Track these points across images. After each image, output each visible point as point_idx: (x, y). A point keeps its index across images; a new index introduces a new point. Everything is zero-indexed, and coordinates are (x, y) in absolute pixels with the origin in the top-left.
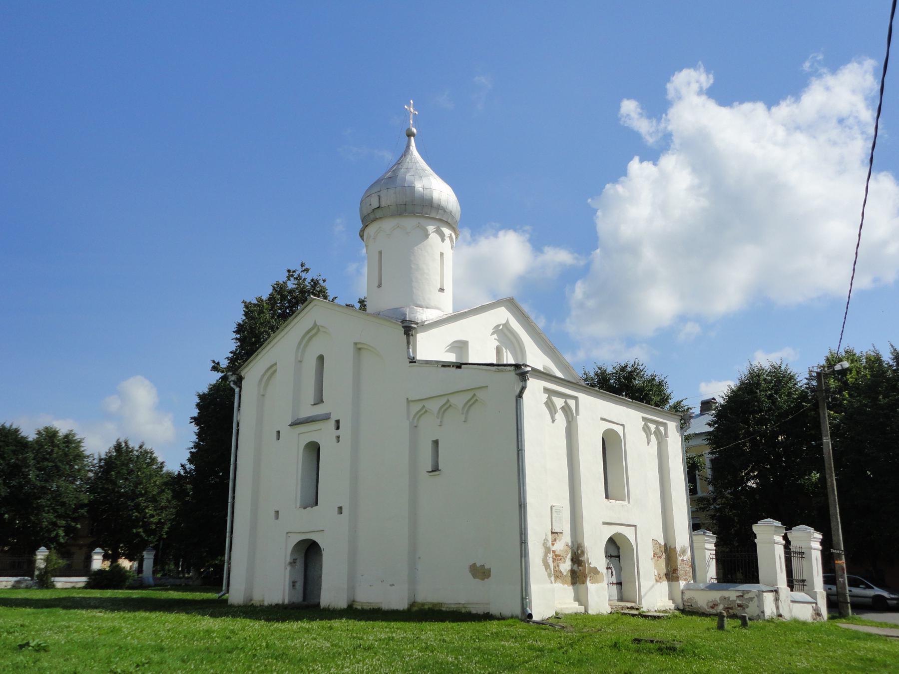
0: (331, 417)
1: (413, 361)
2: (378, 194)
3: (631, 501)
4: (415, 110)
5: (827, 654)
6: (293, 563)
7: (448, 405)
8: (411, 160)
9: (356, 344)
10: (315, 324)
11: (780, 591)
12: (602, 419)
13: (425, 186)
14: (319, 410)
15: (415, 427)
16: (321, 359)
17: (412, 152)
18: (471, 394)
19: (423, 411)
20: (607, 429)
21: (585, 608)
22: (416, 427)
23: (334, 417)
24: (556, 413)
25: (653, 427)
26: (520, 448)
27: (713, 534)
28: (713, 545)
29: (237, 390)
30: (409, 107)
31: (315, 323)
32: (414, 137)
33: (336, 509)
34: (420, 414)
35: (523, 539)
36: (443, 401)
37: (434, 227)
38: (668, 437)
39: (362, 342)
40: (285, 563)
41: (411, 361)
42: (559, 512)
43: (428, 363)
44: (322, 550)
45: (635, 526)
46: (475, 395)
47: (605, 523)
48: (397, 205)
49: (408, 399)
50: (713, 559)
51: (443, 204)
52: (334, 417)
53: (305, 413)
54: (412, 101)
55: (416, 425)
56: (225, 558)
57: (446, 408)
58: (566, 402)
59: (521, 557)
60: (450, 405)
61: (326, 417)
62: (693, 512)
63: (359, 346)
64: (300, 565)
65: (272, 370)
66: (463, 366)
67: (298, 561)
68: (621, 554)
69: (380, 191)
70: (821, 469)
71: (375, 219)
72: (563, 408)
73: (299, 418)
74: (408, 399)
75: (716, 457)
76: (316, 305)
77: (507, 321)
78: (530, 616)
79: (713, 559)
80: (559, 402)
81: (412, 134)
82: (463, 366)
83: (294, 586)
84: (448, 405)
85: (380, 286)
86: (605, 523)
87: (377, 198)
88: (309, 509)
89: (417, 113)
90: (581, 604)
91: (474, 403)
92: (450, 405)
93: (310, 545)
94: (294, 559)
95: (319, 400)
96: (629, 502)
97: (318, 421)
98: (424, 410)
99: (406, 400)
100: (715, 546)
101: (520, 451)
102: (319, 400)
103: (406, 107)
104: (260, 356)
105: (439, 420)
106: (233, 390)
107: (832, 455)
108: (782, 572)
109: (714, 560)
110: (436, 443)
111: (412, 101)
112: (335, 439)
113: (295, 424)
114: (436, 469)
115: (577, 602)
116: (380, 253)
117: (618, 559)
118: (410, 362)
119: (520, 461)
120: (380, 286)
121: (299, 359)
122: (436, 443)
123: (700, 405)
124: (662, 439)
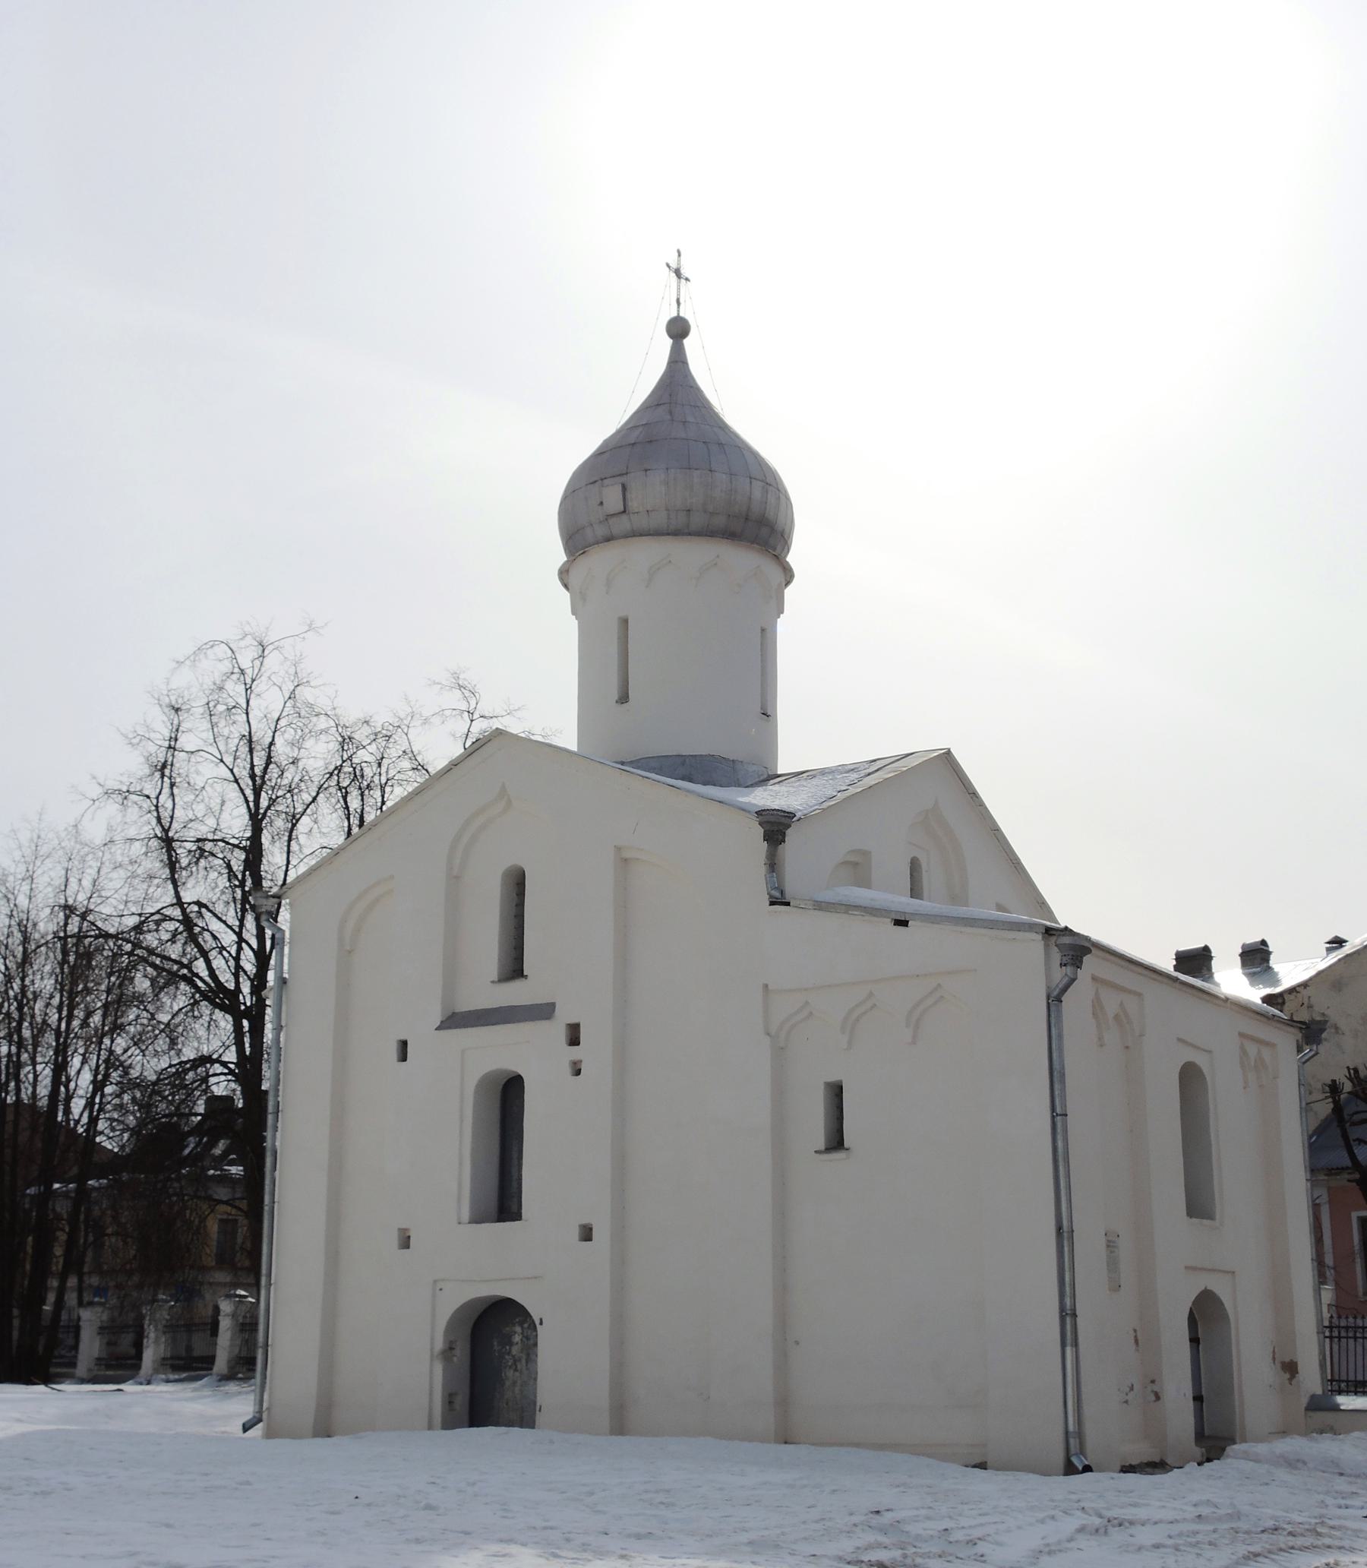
2: (623, 479)
6: (450, 1348)
9: (618, 849)
10: (503, 788)
14: (515, 994)
15: (780, 1052)
16: (517, 884)
20: (1188, 1062)
23: (564, 1016)
25: (1252, 1049)
26: (1058, 1110)
33: (576, 1233)
35: (1068, 1307)
40: (432, 1349)
44: (537, 1322)
48: (1340, 991)
52: (564, 1016)
59: (1063, 1345)
61: (544, 1012)
63: (627, 854)
64: (462, 1353)
69: (627, 473)
72: (1116, 1017)
73: (457, 1011)
75: (250, 875)
83: (450, 1403)
87: (619, 488)
95: (514, 969)
102: (514, 969)
110: (836, 1092)
112: (567, 1070)
113: (454, 1021)
114: (836, 1142)
116: (624, 698)
118: (772, 903)
119: (1059, 1137)
122: (836, 1092)
123: (1174, 963)
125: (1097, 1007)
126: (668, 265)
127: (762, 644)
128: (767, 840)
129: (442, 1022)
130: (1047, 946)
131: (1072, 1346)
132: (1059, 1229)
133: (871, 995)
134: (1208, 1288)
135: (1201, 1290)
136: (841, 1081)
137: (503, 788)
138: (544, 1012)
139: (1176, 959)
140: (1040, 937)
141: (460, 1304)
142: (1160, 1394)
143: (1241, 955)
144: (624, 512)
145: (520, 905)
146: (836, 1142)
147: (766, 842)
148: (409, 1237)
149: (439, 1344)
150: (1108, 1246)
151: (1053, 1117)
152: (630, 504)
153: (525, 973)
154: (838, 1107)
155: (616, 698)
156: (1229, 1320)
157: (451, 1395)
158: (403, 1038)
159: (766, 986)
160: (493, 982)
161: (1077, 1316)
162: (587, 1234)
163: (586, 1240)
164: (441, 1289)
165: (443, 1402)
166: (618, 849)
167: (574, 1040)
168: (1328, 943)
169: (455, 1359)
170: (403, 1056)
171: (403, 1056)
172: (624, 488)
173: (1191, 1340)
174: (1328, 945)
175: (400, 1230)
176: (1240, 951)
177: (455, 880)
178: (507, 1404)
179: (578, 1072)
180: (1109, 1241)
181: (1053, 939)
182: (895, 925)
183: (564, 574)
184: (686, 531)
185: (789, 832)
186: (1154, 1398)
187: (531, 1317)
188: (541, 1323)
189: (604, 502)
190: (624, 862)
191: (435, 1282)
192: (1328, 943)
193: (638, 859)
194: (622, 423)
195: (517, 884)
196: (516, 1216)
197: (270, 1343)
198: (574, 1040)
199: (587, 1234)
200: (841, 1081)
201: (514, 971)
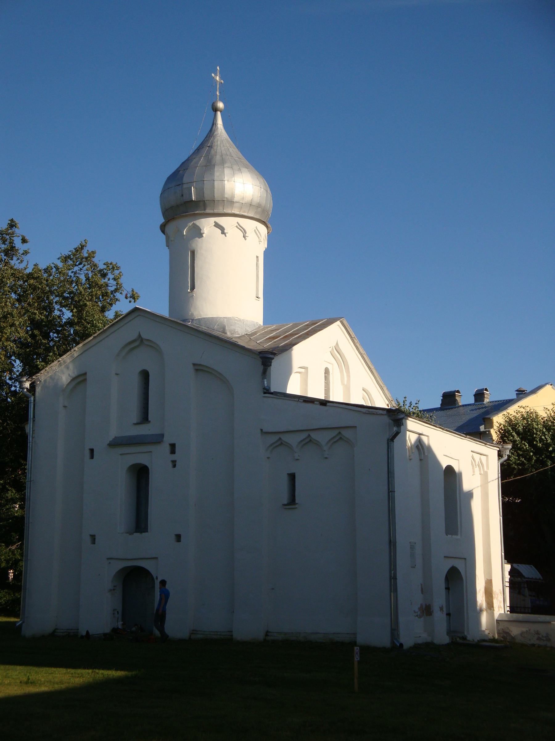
1: (267, 391)
9: (194, 365)
19: (281, 443)
20: (448, 465)
23: (168, 440)
25: (477, 457)
31: (140, 335)
36: (304, 435)
39: (202, 363)
41: (265, 391)
44: (155, 577)
45: (465, 559)
46: (340, 433)
49: (262, 430)
54: (218, 68)
56: (21, 584)
57: (309, 441)
58: (480, 459)
59: (391, 591)
60: (310, 440)
61: (157, 439)
62: (171, 451)
66: (328, 404)
70: (535, 471)
74: (262, 430)
76: (140, 315)
77: (337, 344)
82: (328, 404)
88: (128, 534)
92: (310, 440)
94: (114, 586)
95: (145, 418)
97: (145, 443)
98: (279, 443)
99: (259, 431)
102: (145, 418)
106: (28, 402)
107: (285, 335)
108: (489, 584)
109: (508, 588)
111: (218, 68)
112: (171, 465)
118: (265, 393)
123: (442, 398)
127: (257, 264)
128: (263, 365)
131: (185, 322)
132: (390, 541)
134: (454, 566)
136: (295, 473)
138: (157, 439)
143: (475, 395)
147: (263, 366)
150: (411, 548)
151: (389, 493)
153: (149, 420)
156: (463, 580)
161: (397, 579)
167: (173, 451)
168: (516, 391)
173: (446, 588)
174: (517, 392)
176: (475, 393)
179: (174, 466)
180: (411, 546)
182: (320, 405)
183: (163, 228)
185: (273, 361)
196: (145, 530)
198: (173, 451)
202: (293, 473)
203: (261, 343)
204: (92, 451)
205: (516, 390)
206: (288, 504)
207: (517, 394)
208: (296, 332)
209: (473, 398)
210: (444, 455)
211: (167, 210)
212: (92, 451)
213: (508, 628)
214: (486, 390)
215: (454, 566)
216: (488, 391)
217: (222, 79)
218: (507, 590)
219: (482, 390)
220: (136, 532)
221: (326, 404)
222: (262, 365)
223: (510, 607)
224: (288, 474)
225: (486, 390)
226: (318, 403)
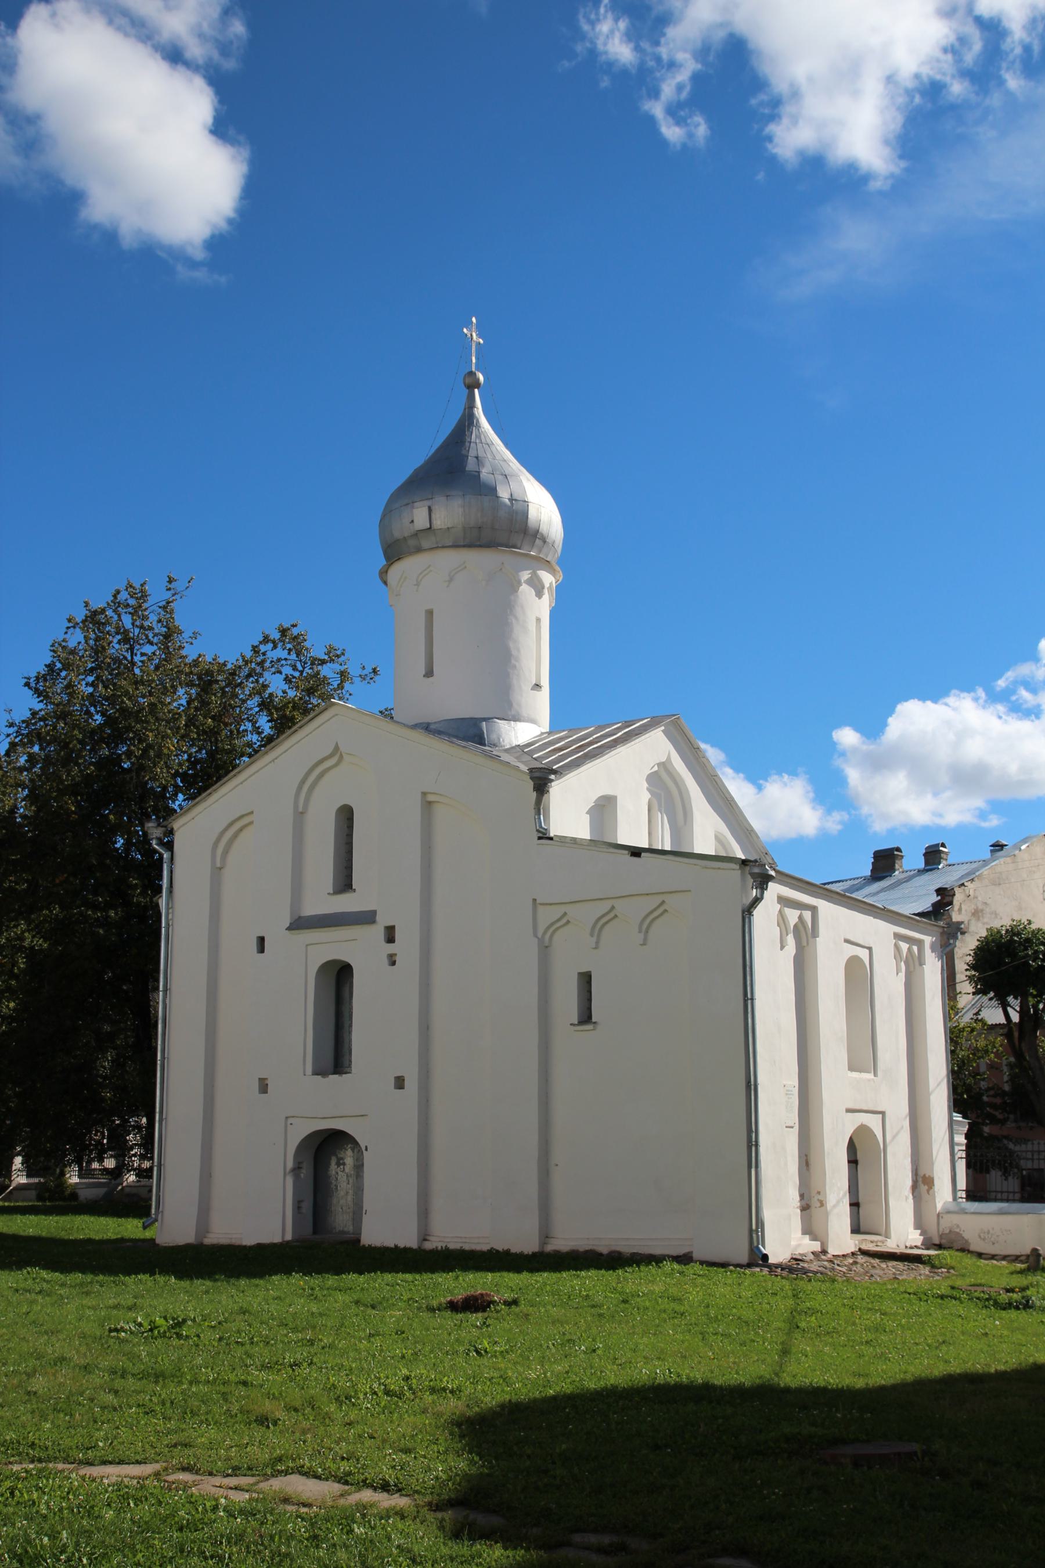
0: (378, 918)
1: (544, 836)
3: (879, 1073)
4: (479, 336)
5: (804, 1380)
6: (297, 1169)
7: (612, 915)
8: (479, 437)
9: (424, 794)
10: (337, 748)
11: (861, 1205)
12: (847, 941)
13: (515, 497)
14: (345, 903)
15: (545, 949)
16: (346, 816)
17: (478, 421)
18: (563, 909)
21: (822, 1244)
22: (547, 947)
23: (383, 920)
24: (787, 935)
25: (904, 946)
27: (963, 1118)
28: (964, 1136)
29: (166, 856)
30: (470, 330)
32: (478, 388)
33: (392, 1082)
34: (555, 927)
37: (529, 572)
38: (925, 964)
41: (541, 835)
42: (791, 1094)
43: (563, 840)
44: (363, 1149)
45: (883, 1113)
47: (848, 1111)
50: (961, 1158)
51: (543, 529)
52: (383, 920)
53: (311, 908)
54: (474, 320)
55: (547, 945)
61: (367, 918)
63: (430, 798)
64: (307, 1172)
65: (240, 824)
67: (304, 1165)
68: (859, 1157)
71: (419, 550)
72: (795, 926)
73: (302, 915)
78: (765, 1257)
79: (961, 1158)
80: (792, 916)
81: (477, 385)
83: (299, 1208)
84: (612, 915)
85: (429, 673)
86: (848, 1111)
87: (425, 510)
89: (481, 341)
90: (814, 1238)
91: (661, 914)
93: (323, 1141)
95: (345, 883)
96: (875, 1075)
99: (419, 797)
100: (966, 1139)
101: (747, 999)
102: (345, 883)
103: (465, 330)
104: (215, 796)
105: (594, 939)
111: (474, 320)
113: (299, 924)
114: (586, 1017)
115: (808, 1236)
117: (854, 1165)
118: (540, 838)
120: (429, 673)
121: (300, 810)
123: (873, 860)
124: (914, 968)
125: (782, 918)
126: (329, 894)
129: (291, 924)
130: (743, 874)
133: (613, 908)
135: (858, 1125)
136: (590, 972)
137: (337, 748)
138: (367, 918)
139: (874, 858)
140: (737, 867)
141: (305, 1136)
142: (824, 1202)
143: (925, 855)
144: (430, 528)
145: (350, 835)
146: (586, 1017)
148: (267, 1085)
149: (290, 1164)
152: (434, 522)
153: (354, 888)
154: (588, 991)
155: (424, 673)
157: (300, 1202)
158: (261, 935)
159: (535, 900)
160: (329, 894)
162: (400, 1083)
163: (400, 1089)
164: (291, 1124)
165: (293, 1204)
166: (424, 794)
167: (390, 938)
168: (991, 846)
169: (302, 1175)
170: (261, 949)
171: (261, 949)
172: (430, 509)
174: (992, 848)
175: (260, 1079)
176: (924, 851)
177: (300, 816)
178: (342, 1208)
179: (393, 963)
181: (747, 869)
182: (631, 856)
184: (478, 543)
186: (819, 1205)
187: (359, 1146)
188: (366, 1150)
189: (415, 521)
190: (428, 805)
191: (287, 1118)
192: (991, 846)
193: (438, 802)
194: (433, 450)
195: (346, 816)
197: (162, 1163)
198: (390, 938)
199: (400, 1083)
200: (590, 972)
201: (346, 885)
202: (587, 972)
203: (539, 757)
204: (261, 940)
205: (991, 844)
206: (581, 1022)
207: (992, 851)
208: (596, 740)
209: (922, 859)
210: (690, 891)
211: (389, 546)
212: (261, 940)
213: (958, 1226)
214: (943, 845)
215: (864, 1123)
216: (945, 847)
217: (480, 338)
218: (961, 1166)
219: (937, 845)
220: (335, 1073)
221: (641, 854)
222: (534, 791)
223: (967, 1191)
224: (580, 974)
225: (943, 845)
226: (626, 852)
